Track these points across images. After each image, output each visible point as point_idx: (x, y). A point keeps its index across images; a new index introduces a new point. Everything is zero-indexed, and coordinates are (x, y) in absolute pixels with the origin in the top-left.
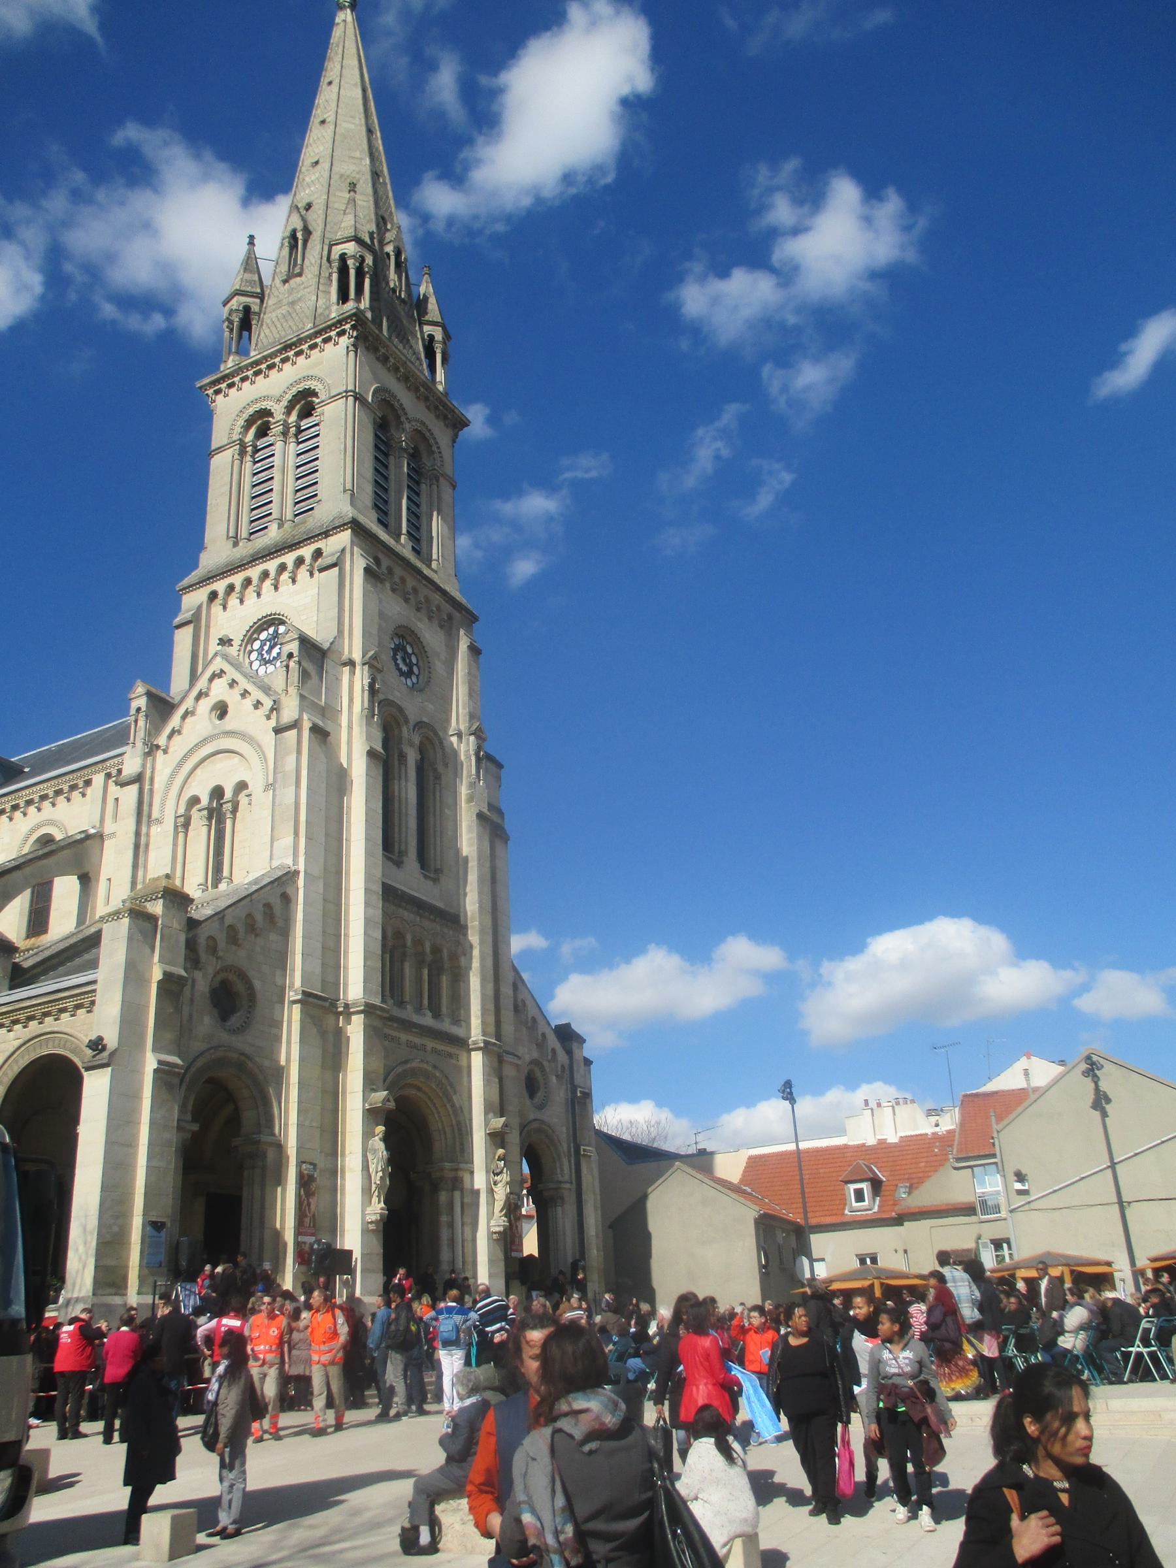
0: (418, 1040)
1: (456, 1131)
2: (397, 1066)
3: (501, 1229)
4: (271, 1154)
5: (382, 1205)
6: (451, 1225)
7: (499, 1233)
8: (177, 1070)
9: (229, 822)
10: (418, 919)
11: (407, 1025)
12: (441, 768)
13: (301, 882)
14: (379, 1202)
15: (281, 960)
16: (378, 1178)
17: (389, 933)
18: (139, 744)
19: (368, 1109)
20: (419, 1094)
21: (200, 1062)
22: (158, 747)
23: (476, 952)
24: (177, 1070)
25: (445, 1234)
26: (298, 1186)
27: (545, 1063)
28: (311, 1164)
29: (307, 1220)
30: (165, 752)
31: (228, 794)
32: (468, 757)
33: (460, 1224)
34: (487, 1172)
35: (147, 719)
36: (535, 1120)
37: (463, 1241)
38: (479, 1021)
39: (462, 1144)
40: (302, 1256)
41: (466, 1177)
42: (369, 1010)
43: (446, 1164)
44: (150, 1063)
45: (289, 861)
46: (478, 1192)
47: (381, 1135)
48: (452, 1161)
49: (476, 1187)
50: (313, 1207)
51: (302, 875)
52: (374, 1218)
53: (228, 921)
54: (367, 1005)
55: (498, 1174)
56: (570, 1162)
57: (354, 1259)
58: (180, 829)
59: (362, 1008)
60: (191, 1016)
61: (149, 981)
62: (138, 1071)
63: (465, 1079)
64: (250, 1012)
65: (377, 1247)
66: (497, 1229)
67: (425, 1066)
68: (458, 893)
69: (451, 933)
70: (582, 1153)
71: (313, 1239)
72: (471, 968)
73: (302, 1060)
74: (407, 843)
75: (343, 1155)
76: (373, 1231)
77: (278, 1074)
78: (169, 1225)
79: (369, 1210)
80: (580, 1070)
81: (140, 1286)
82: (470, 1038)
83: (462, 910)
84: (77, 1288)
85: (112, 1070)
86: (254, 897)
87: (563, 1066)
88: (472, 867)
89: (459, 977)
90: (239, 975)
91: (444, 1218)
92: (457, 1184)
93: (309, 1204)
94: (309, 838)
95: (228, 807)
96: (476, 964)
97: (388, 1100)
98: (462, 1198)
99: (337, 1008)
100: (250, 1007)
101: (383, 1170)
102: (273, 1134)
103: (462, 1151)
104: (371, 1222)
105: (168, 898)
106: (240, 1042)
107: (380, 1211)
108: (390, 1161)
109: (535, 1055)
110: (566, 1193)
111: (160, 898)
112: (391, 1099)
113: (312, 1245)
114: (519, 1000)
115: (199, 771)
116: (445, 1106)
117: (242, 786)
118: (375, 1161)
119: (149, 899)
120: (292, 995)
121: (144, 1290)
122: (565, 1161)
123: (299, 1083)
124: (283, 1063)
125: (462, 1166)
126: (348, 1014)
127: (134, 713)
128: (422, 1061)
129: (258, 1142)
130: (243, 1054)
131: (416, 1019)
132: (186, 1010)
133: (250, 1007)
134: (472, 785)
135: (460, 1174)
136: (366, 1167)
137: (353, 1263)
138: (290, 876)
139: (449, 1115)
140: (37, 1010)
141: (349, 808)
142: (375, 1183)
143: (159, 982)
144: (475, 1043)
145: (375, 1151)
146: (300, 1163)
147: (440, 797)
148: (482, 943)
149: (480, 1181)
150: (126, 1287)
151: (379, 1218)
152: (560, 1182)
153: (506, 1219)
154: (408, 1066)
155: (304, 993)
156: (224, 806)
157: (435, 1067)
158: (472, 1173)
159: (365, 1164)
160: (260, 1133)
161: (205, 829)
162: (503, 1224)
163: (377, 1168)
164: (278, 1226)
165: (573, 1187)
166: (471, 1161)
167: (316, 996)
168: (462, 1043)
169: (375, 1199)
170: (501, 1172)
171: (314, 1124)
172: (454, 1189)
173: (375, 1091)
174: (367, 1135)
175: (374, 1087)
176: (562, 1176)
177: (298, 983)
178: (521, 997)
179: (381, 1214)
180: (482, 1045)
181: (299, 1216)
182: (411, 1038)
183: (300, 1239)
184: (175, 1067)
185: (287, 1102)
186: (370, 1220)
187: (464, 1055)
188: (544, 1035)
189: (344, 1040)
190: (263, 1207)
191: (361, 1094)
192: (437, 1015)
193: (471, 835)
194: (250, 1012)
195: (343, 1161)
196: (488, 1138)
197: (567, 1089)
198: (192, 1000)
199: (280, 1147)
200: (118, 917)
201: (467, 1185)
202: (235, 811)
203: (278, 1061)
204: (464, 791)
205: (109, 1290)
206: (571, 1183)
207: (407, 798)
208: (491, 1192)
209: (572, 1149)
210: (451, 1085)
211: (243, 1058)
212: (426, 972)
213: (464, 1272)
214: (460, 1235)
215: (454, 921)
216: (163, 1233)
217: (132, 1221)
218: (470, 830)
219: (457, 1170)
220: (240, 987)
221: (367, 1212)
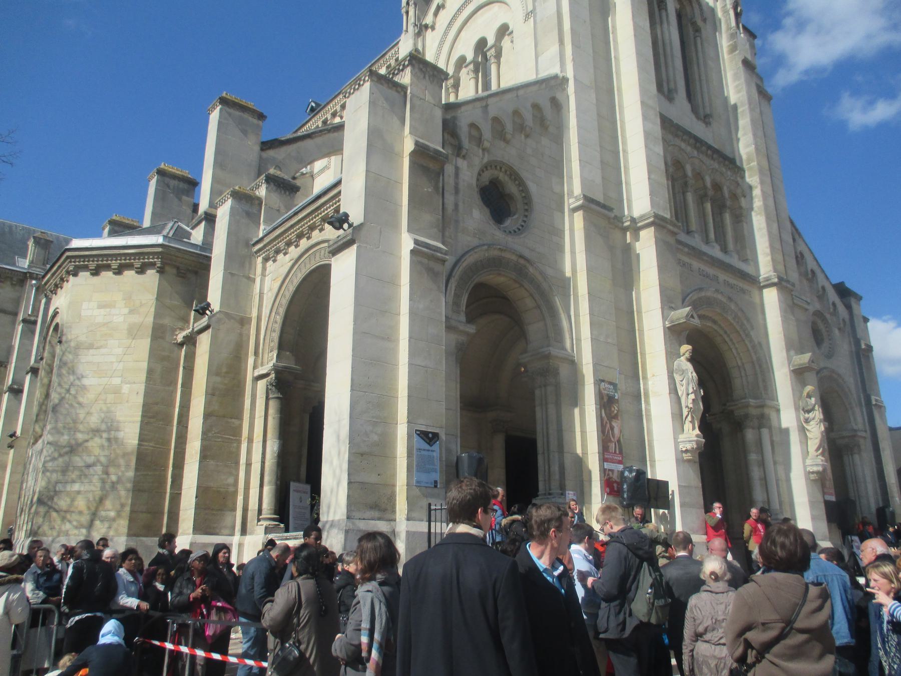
0: (711, 271)
1: (757, 367)
2: (691, 292)
3: (820, 469)
4: (564, 371)
5: (697, 431)
6: (762, 464)
7: (817, 473)
8: (439, 254)
9: (493, 68)
10: (696, 152)
11: (698, 254)
12: (700, 23)
13: (571, 88)
14: (694, 428)
15: (557, 166)
16: (690, 401)
17: (670, 163)
18: (411, 28)
19: (669, 328)
20: (715, 327)
21: (470, 260)
22: (426, 27)
23: (757, 192)
24: (439, 254)
25: (756, 473)
26: (598, 407)
27: (828, 316)
28: (610, 383)
29: (612, 446)
30: (433, 28)
31: (491, 41)
32: (726, 12)
33: (772, 463)
34: (797, 409)
35: (416, 6)
36: (825, 368)
37: (777, 481)
38: (769, 258)
39: (764, 381)
40: (611, 486)
41: (773, 415)
42: (658, 223)
43: (750, 400)
44: (407, 243)
45: (555, 70)
46: (787, 431)
47: (687, 355)
48: (756, 398)
49: (784, 425)
50: (616, 431)
51: (571, 83)
52: (689, 446)
53: (493, 112)
54: (656, 216)
55: (809, 412)
56: (862, 412)
57: (670, 492)
58: (450, 90)
59: (652, 219)
60: (456, 206)
61: (400, 156)
62: (392, 253)
63: (760, 316)
64: (526, 216)
65: (695, 480)
66: (815, 469)
67: (720, 297)
68: (732, 140)
69: (729, 173)
70: (874, 403)
71: (621, 467)
72: (752, 209)
73: (590, 270)
74: (675, 83)
75: (645, 378)
76: (689, 461)
77: (565, 286)
78: (443, 436)
79: (682, 437)
80: (858, 322)
81: (410, 510)
82: (760, 276)
83: (737, 154)
84: (332, 510)
85: (357, 247)
86: (521, 92)
87: (844, 320)
88: (743, 111)
89: (741, 217)
90: (511, 175)
91: (753, 457)
92: (763, 421)
93: (612, 428)
94: (576, 45)
95: (491, 53)
96: (758, 203)
97: (692, 316)
98: (771, 436)
99: (623, 223)
100: (526, 210)
101: (694, 392)
102: (564, 349)
103: (766, 388)
104: (686, 451)
105: (416, 65)
106: (520, 244)
107: (696, 439)
108: (701, 383)
109: (817, 306)
110: (862, 441)
111: (408, 66)
112: (695, 316)
113: (622, 473)
114: (798, 252)
115: (463, 34)
116: (744, 341)
117: (504, 30)
118: (684, 382)
119: (396, 72)
120: (570, 202)
121: (414, 515)
122: (857, 410)
123: (589, 293)
124: (568, 273)
125: (768, 402)
126: (636, 228)
127: (405, 5)
128: (717, 291)
129: (548, 357)
130: (521, 256)
131: (704, 248)
132: (450, 199)
133: (526, 210)
134: (733, 36)
135: (766, 411)
136: (673, 390)
137: (670, 497)
138: (556, 83)
139: (748, 350)
140: (304, 225)
141: (614, 27)
142: (687, 407)
143: (413, 154)
144: (767, 279)
145: (683, 372)
146: (598, 382)
147: (702, 48)
148: (762, 183)
149: (788, 418)
150: (394, 511)
151: (695, 446)
152: (855, 431)
153: (823, 458)
154: (703, 294)
155: (586, 198)
156: (488, 54)
157: (730, 299)
158: (778, 411)
159: (672, 386)
160: (549, 346)
161: (473, 82)
162: (821, 463)
163: (687, 389)
164: (579, 451)
165: (868, 435)
166: (775, 398)
167: (598, 203)
168: (752, 280)
169: (688, 426)
170: (813, 409)
171: (609, 340)
172: (760, 427)
173: (674, 309)
174: (672, 355)
175: (673, 305)
176: (856, 425)
177: (577, 190)
178: (800, 249)
179: (697, 442)
180: (776, 280)
181: (603, 441)
182: (703, 267)
183: (607, 466)
184: (437, 251)
185: (577, 315)
186: (684, 449)
187: (755, 292)
188: (823, 288)
189: (634, 258)
190: (560, 431)
191: (659, 311)
192: (725, 250)
193: (737, 83)
194: (526, 216)
195: (645, 384)
196: (792, 374)
197: (850, 342)
198: (457, 190)
199: (573, 364)
200: (359, 85)
201: (774, 423)
202: (498, 56)
203: (562, 273)
204: (724, 42)
205: (369, 514)
206: (866, 431)
207: (671, 40)
208: (803, 430)
209: (862, 400)
210: (748, 320)
211: (522, 261)
212: (708, 206)
213: (782, 513)
214: (774, 475)
215: (731, 163)
216: (436, 447)
217: (396, 428)
218: (736, 77)
219: (762, 406)
220: (512, 188)
221: (679, 440)
